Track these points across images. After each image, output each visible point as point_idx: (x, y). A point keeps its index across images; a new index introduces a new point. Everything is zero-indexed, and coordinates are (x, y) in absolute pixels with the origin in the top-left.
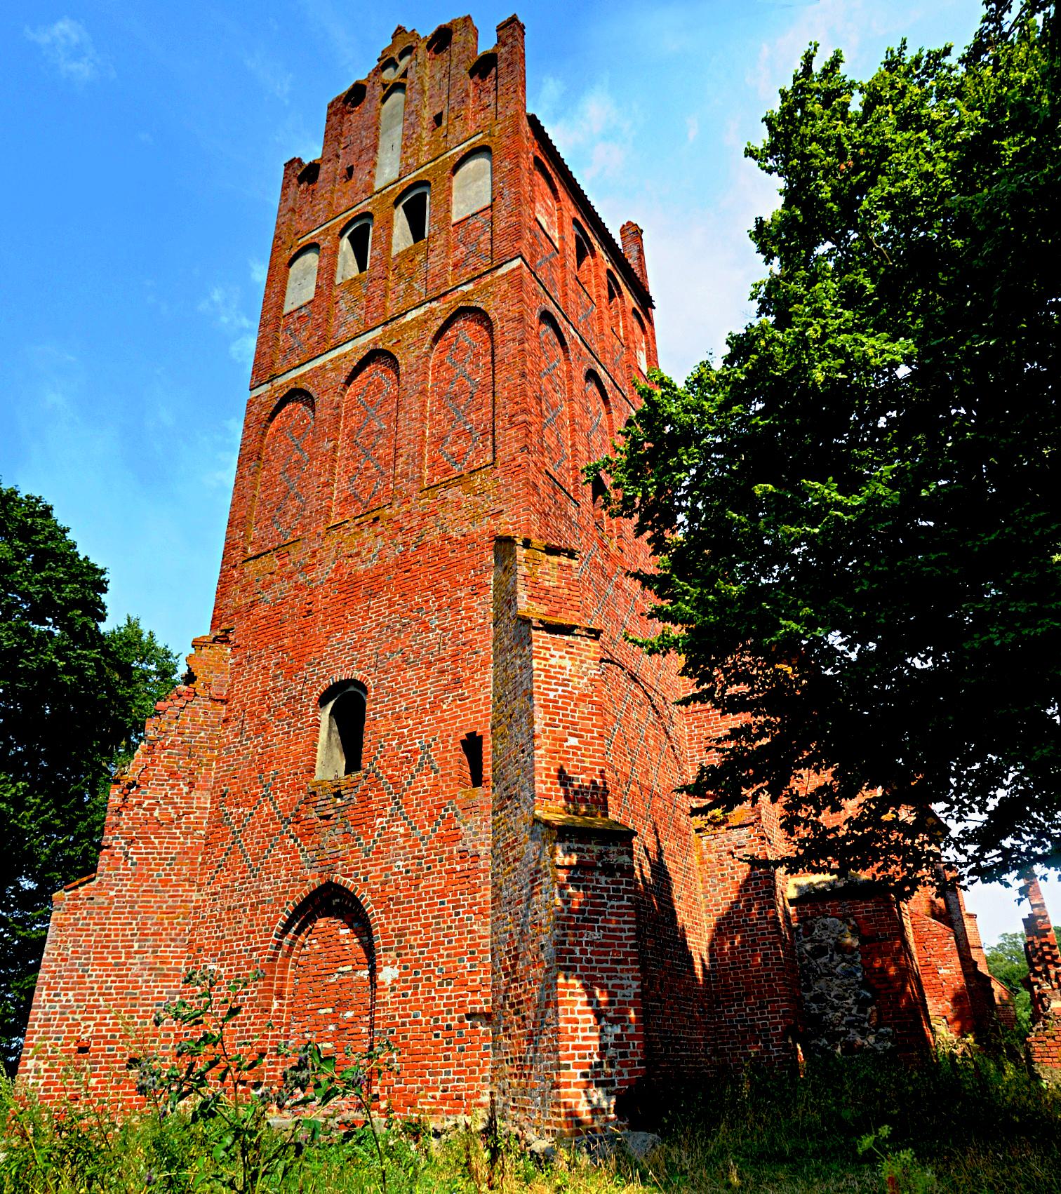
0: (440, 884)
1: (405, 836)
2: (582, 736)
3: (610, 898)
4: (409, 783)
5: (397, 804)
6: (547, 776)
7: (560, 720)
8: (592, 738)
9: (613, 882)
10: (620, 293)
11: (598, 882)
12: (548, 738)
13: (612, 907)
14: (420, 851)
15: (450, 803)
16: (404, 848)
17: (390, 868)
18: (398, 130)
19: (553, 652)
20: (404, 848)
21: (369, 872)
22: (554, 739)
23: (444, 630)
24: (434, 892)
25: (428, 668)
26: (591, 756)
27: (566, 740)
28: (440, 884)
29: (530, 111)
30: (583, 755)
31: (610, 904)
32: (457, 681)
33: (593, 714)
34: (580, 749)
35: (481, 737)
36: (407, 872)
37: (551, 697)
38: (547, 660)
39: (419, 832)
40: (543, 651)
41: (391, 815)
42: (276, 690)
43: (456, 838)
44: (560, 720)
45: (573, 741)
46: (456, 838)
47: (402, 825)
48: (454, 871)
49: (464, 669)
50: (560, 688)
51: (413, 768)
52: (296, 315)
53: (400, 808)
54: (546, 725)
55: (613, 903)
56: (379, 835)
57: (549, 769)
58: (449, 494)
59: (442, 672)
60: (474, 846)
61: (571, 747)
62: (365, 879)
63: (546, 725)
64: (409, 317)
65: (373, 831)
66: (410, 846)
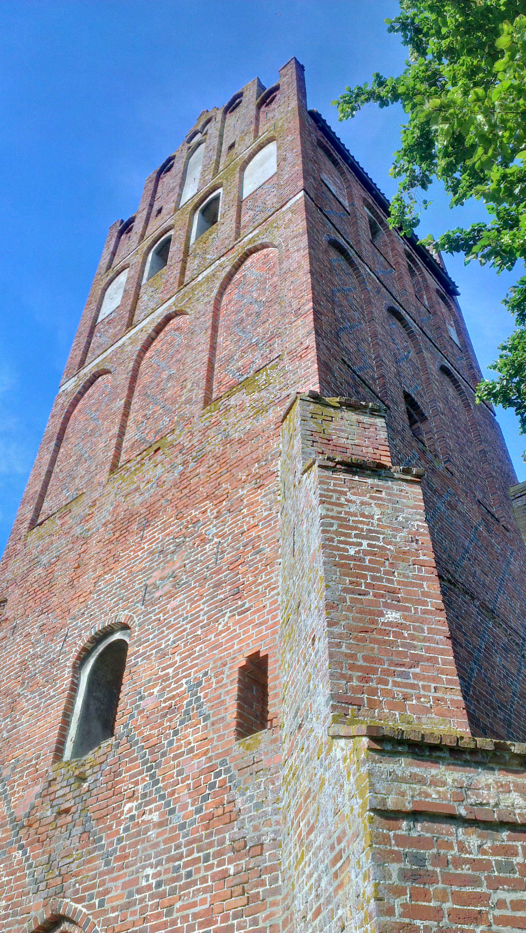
0: (203, 901)
1: (160, 824)
2: (408, 609)
3: (495, 884)
4: (171, 743)
5: (152, 776)
6: (352, 667)
7: (367, 585)
8: (425, 612)
9: (496, 851)
10: (419, 269)
11: (462, 848)
12: (349, 609)
13: (501, 904)
14: (178, 847)
15: (222, 763)
16: (157, 845)
17: (136, 881)
18: (200, 168)
19: (349, 496)
20: (157, 845)
21: (107, 892)
22: (361, 612)
23: (223, 536)
24: (195, 916)
25: (202, 586)
26: (425, 640)
27: (381, 614)
28: (203, 901)
29: (308, 109)
30: (413, 637)
31: (495, 897)
32: (237, 593)
33: (422, 578)
34: (407, 628)
35: (267, 656)
36: (159, 885)
37: (352, 552)
38: (341, 505)
39: (176, 820)
40: (335, 495)
41: (144, 796)
42: (35, 657)
43: (232, 817)
44: (367, 585)
45: (392, 616)
46: (232, 817)
47: (157, 809)
48: (224, 876)
49: (245, 574)
50: (365, 543)
51: (176, 721)
52: (106, 321)
53: (157, 782)
54: (346, 590)
55: (501, 895)
56: (126, 829)
57: (353, 656)
58: (232, 401)
59: (218, 585)
60: (256, 828)
61: (390, 624)
62: (102, 904)
63: (346, 590)
64: (200, 278)
65: (119, 824)
66: (165, 842)
